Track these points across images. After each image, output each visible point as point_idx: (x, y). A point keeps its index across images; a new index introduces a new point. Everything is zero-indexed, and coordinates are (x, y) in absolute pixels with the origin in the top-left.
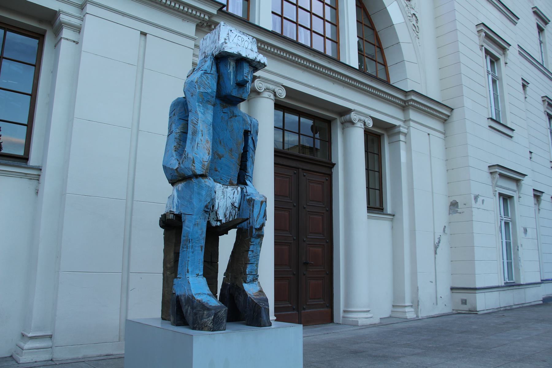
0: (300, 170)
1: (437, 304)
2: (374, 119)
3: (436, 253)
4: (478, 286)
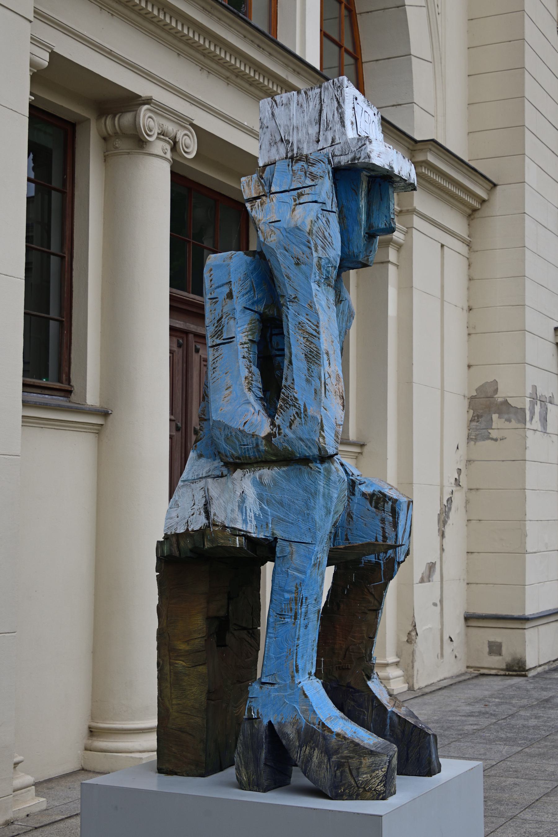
0: (191, 336)
1: (442, 655)
2: (202, 135)
3: (443, 535)
4: (529, 611)
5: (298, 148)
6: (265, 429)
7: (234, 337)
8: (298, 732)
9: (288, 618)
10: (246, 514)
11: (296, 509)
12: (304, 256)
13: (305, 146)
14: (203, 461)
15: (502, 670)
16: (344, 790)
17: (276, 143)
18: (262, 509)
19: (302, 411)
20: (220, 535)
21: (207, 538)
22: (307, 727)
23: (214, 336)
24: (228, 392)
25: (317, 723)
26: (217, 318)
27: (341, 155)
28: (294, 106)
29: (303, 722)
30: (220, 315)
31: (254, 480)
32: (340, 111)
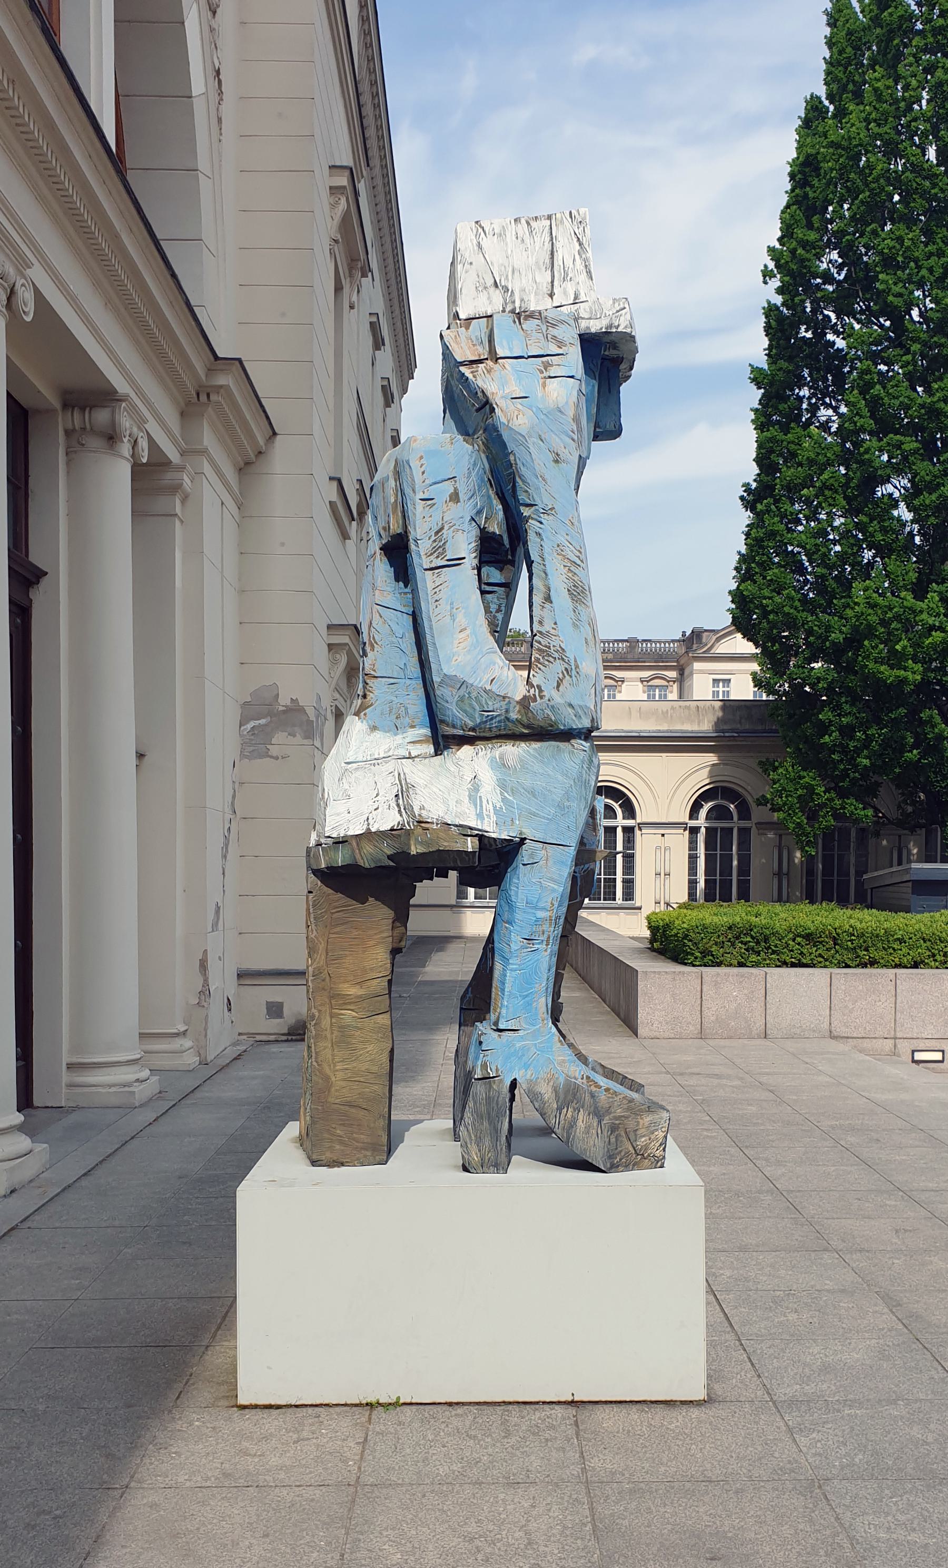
5: (522, 300)
6: (520, 692)
7: (464, 558)
8: (556, 1090)
9: (539, 944)
10: (481, 806)
11: (553, 800)
12: (566, 451)
13: (532, 297)
14: (378, 736)
15: (283, 1035)
16: (621, 1160)
17: (485, 288)
18: (504, 800)
19: (573, 667)
20: (442, 835)
21: (417, 839)
22: (568, 1083)
23: (431, 554)
24: (462, 635)
25: (580, 1077)
26: (436, 528)
27: (590, 319)
28: (510, 236)
29: (562, 1080)
30: (440, 524)
31: (493, 760)
32: (584, 256)
